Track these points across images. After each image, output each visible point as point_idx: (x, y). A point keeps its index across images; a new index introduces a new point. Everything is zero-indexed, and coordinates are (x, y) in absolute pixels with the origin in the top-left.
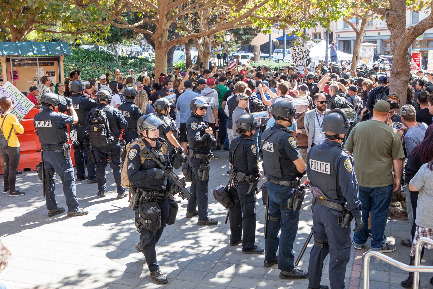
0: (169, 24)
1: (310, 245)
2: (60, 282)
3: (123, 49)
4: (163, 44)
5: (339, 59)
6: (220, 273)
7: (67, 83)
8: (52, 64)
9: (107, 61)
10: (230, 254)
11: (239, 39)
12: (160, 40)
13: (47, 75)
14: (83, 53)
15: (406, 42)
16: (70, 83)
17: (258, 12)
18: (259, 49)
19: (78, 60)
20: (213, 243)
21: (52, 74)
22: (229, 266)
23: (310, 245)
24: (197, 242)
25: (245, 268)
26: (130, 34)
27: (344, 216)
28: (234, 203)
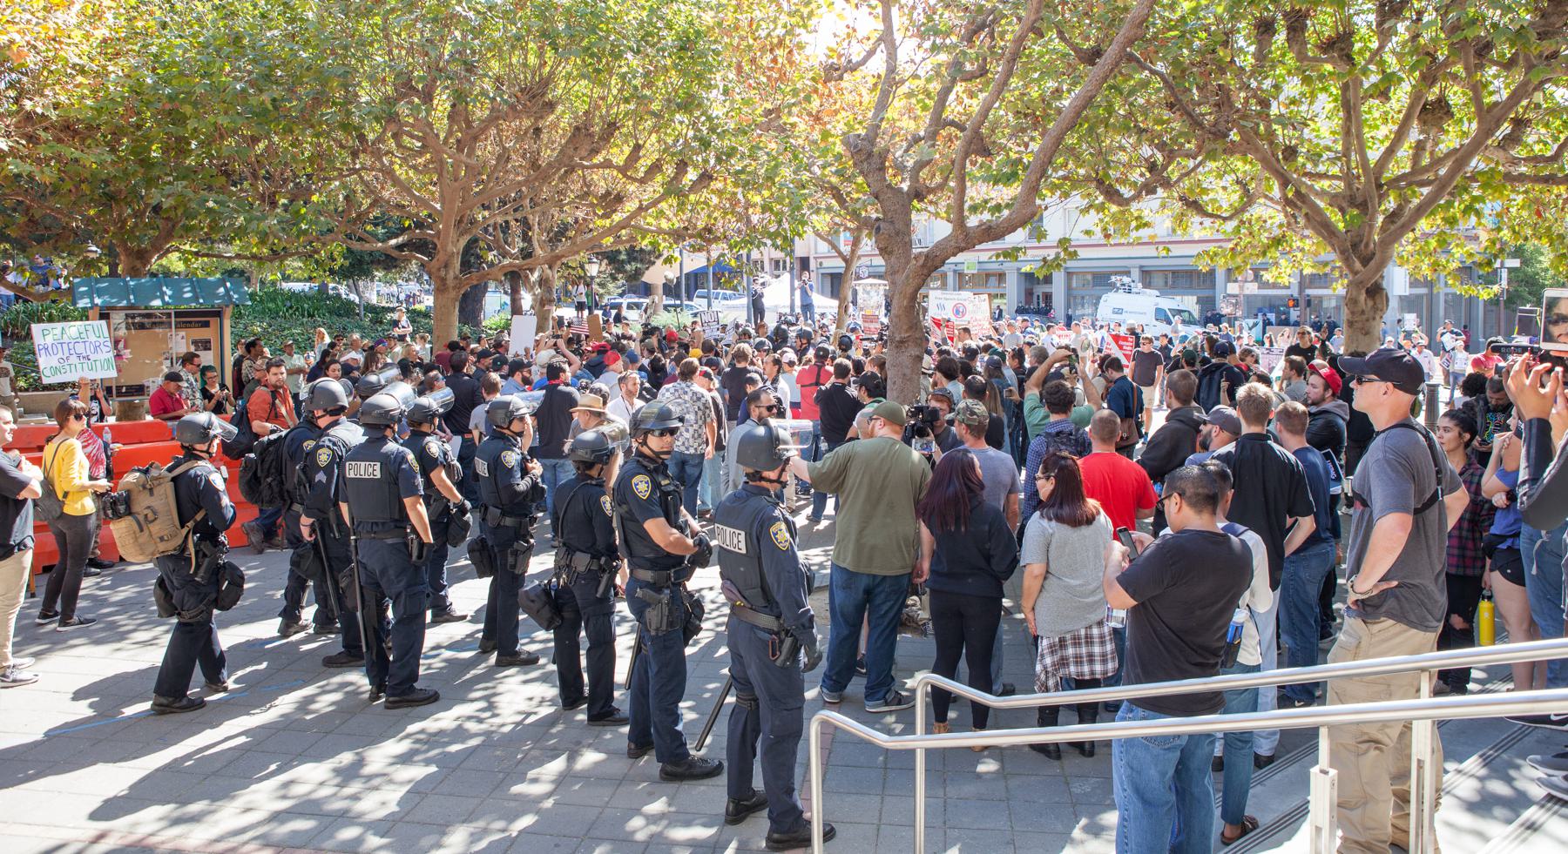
0: (463, 242)
1: (731, 699)
2: (161, 819)
3: (375, 291)
4: (450, 282)
5: (817, 311)
6: (531, 774)
7: (238, 364)
8: (206, 325)
9: (339, 315)
10: (560, 727)
11: (619, 271)
12: (443, 273)
13: (192, 349)
14: (290, 299)
15: (914, 283)
16: (246, 364)
17: (650, 220)
18: (660, 291)
19: (274, 315)
20: (525, 706)
21: (206, 345)
22: (557, 756)
23: (731, 699)
24: (491, 707)
25: (589, 758)
26: (390, 262)
27: (782, 642)
28: (562, 618)
